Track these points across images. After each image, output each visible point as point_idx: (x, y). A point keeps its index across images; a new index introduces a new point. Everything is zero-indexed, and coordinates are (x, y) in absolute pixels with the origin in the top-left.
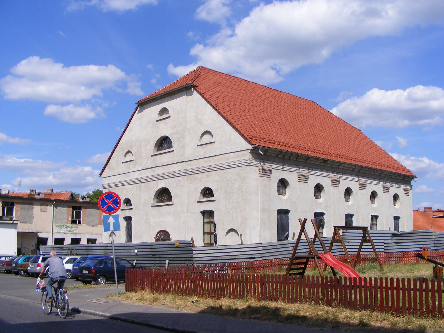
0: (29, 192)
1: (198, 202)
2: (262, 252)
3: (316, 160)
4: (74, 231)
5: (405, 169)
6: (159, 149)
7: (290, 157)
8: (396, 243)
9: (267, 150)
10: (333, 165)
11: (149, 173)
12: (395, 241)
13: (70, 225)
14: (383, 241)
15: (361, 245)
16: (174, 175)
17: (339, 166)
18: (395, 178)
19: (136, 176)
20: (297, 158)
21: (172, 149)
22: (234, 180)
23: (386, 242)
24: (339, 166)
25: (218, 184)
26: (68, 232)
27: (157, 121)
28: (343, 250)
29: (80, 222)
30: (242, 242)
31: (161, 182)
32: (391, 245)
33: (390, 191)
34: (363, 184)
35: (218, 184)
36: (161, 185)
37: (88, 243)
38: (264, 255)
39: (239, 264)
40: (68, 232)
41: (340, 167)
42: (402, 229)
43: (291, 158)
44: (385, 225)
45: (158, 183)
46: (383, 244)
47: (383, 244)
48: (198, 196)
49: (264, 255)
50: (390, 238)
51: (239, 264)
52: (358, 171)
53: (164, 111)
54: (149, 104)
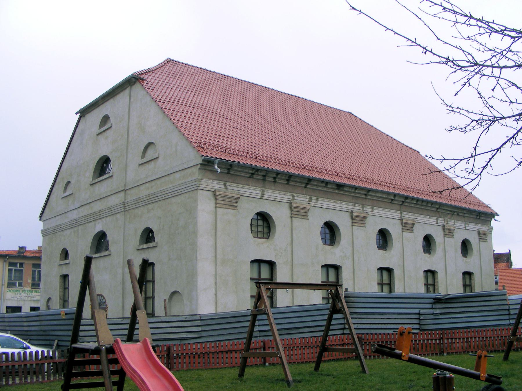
0: (18, 249)
1: (138, 250)
2: (200, 329)
3: (324, 185)
4: (35, 296)
5: (480, 204)
6: (101, 175)
7: (275, 178)
8: (441, 314)
9: (231, 165)
10: (355, 193)
11: (85, 211)
12: (438, 311)
13: (29, 289)
14: (417, 311)
15: (330, 319)
16: (111, 212)
17: (366, 195)
18: (464, 216)
19: (74, 215)
20: (288, 180)
21: (111, 174)
22: (180, 214)
23: (422, 311)
24: (366, 195)
25: (160, 222)
26: (26, 298)
27: (97, 135)
28: (347, 326)
29: (20, 285)
30: (166, 313)
31: (98, 223)
32: (432, 317)
33: (454, 236)
34: (410, 224)
35: (160, 222)
36: (99, 227)
37: (7, 312)
38: (203, 334)
39: (386, 336)
40: (26, 298)
41: (368, 197)
42: (442, 291)
43: (278, 180)
44: (410, 283)
45: (95, 224)
46: (417, 316)
47: (417, 316)
48: (135, 239)
49: (203, 334)
50: (429, 306)
51: (386, 336)
52: (401, 203)
53: (106, 119)
54: (90, 112)
